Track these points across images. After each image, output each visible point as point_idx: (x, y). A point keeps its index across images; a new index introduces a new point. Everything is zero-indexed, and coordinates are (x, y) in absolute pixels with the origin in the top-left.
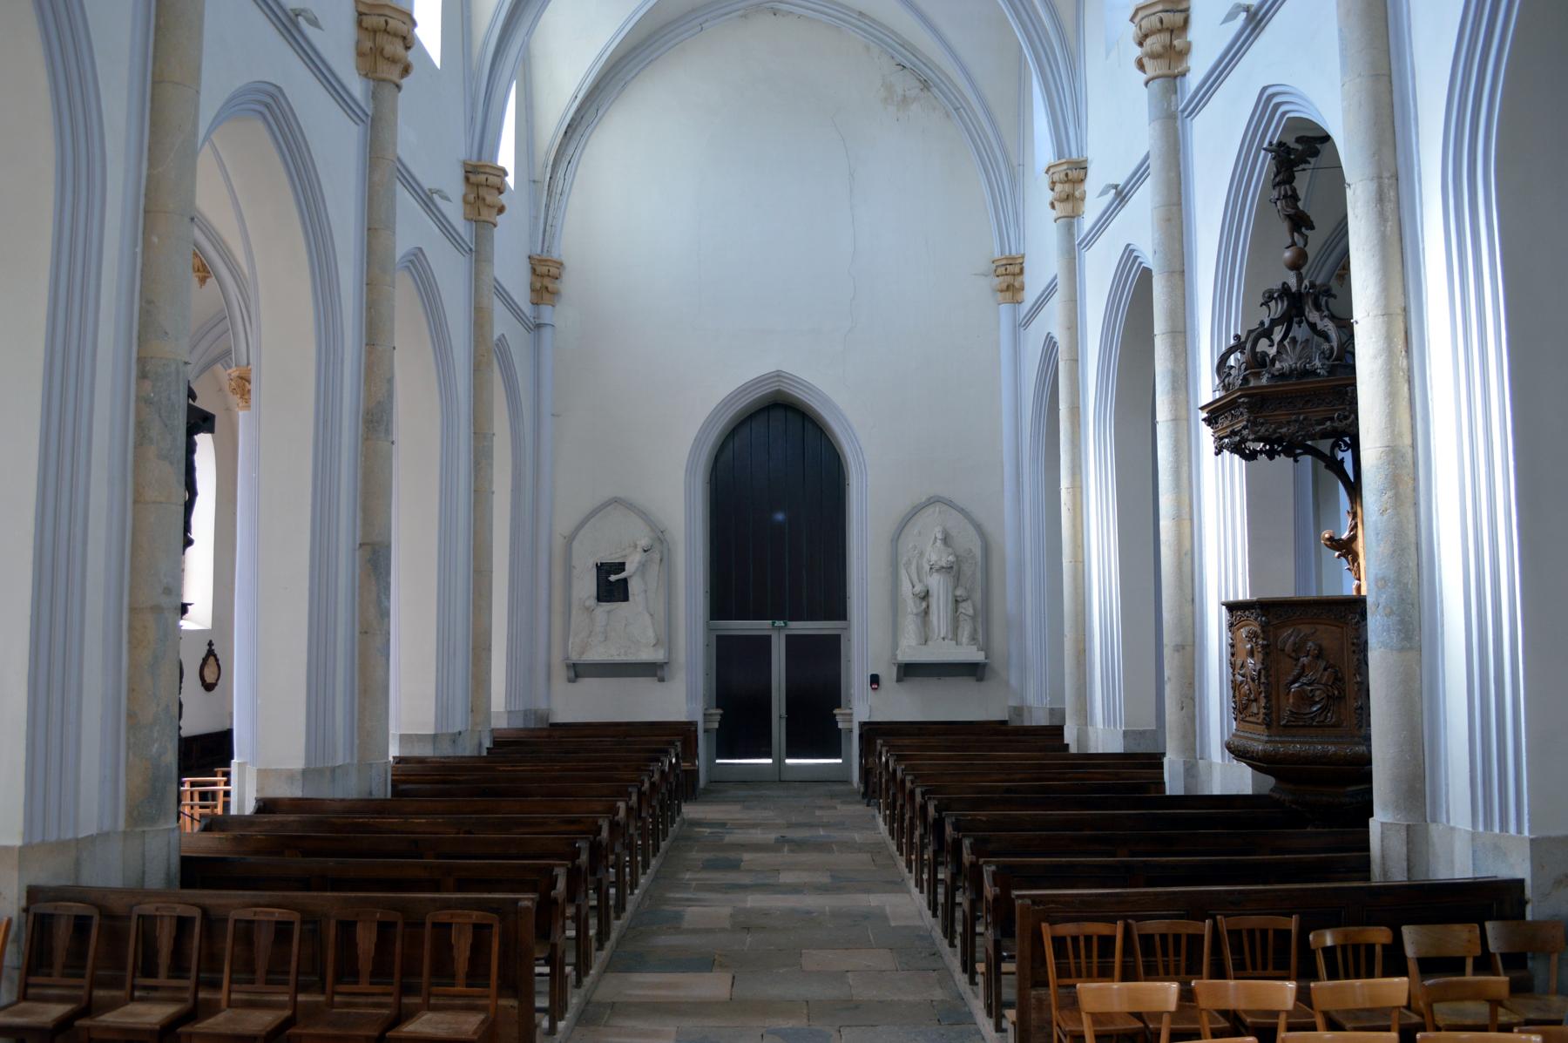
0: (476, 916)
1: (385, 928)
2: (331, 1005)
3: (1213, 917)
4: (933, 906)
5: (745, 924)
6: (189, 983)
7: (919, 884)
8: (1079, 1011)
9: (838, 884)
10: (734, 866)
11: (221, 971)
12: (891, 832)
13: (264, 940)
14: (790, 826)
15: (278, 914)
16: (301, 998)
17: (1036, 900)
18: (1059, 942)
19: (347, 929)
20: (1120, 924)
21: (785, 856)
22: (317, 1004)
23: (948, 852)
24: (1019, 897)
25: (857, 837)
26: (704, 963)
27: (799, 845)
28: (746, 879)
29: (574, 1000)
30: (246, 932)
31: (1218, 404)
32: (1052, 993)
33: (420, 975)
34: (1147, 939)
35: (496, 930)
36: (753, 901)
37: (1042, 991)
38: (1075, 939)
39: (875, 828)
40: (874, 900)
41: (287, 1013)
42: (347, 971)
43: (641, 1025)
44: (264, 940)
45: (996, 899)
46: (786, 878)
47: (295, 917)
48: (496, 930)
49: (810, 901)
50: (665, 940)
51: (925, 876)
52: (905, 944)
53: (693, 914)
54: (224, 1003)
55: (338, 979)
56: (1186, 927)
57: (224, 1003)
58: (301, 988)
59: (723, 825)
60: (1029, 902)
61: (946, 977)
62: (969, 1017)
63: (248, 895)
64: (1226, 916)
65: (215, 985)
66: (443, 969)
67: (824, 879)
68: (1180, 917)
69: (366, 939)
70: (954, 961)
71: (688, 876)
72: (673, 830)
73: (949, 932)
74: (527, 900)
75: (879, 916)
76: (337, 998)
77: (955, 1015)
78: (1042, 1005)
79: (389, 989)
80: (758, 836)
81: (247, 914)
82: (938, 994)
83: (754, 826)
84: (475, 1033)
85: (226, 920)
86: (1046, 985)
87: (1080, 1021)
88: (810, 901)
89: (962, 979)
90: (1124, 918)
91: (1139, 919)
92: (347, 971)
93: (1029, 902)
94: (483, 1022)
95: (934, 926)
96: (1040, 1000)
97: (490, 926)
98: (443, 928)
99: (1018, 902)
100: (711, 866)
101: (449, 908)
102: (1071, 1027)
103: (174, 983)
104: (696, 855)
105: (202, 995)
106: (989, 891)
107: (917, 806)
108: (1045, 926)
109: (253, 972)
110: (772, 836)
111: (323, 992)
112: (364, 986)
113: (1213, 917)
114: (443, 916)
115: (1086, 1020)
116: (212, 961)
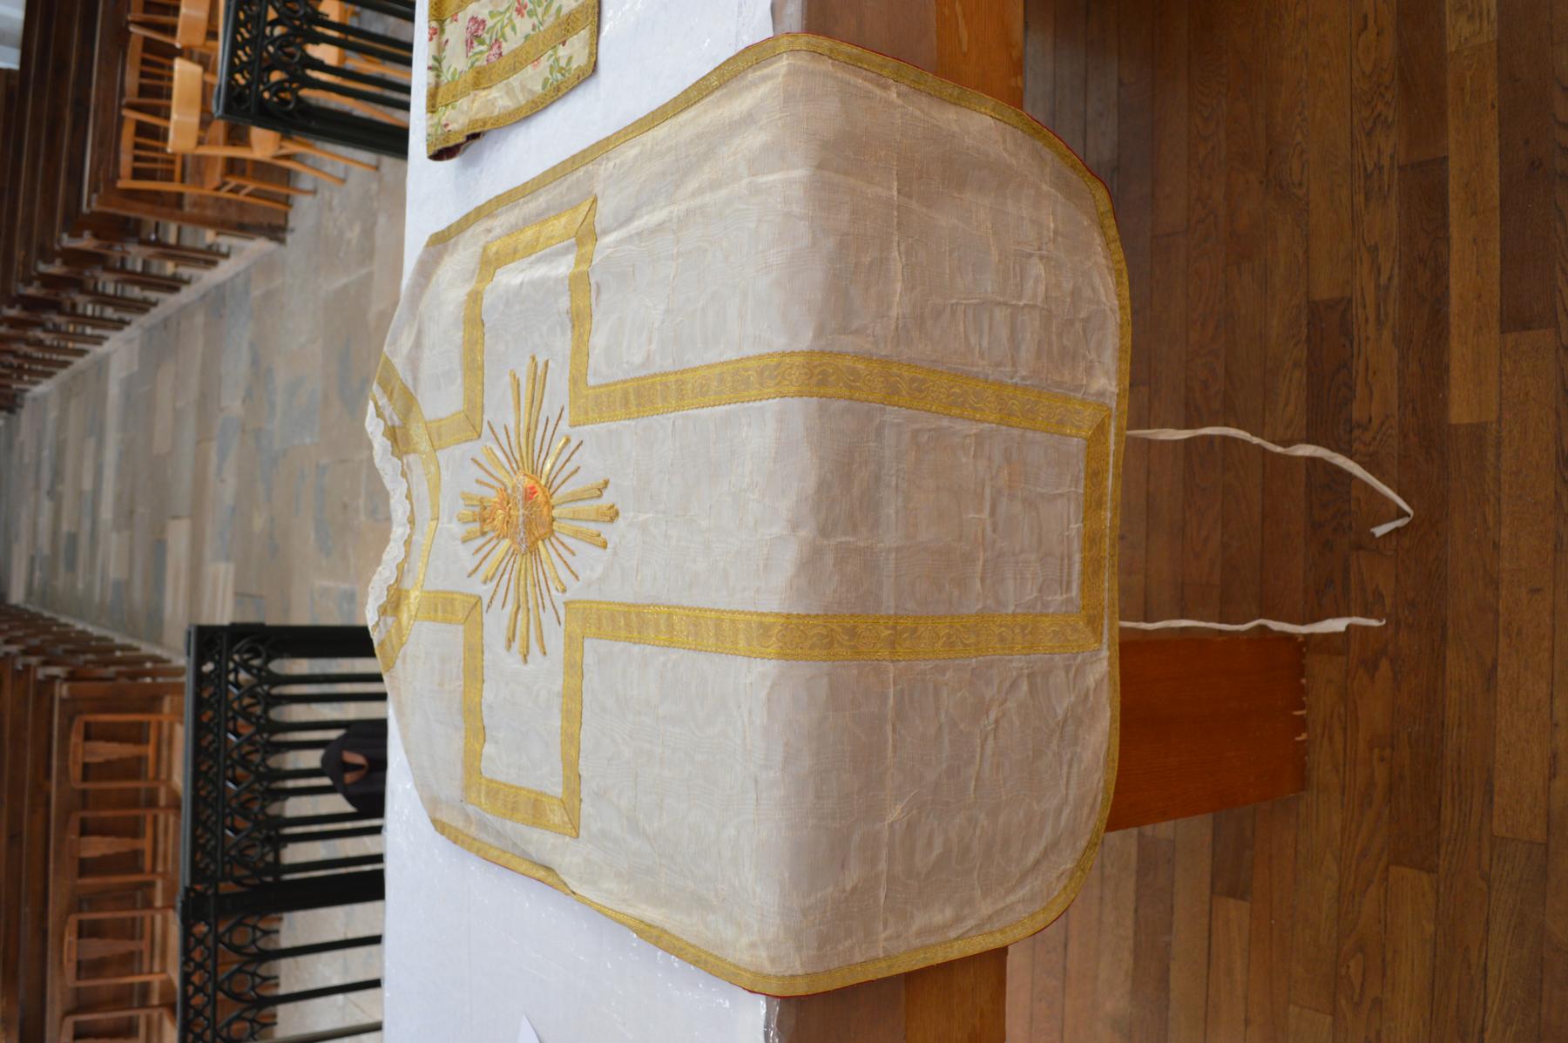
0: (76, 738)
1: (85, 831)
3: (128, 23)
4: (120, 324)
5: (126, 517)
6: (141, 1014)
7: (98, 340)
8: (199, 159)
9: (97, 430)
10: (73, 538)
11: (131, 985)
12: (49, 375)
13: (97, 948)
14: (37, 487)
15: (70, 938)
16: (159, 903)
17: (94, 189)
18: (137, 174)
19: (86, 867)
20: (127, 113)
21: (66, 489)
22: (165, 890)
23: (57, 295)
24: (89, 204)
25: (53, 415)
26: (159, 548)
27: (57, 474)
28: (87, 525)
30: (86, 968)
32: (190, 191)
33: (137, 790)
34: (143, 91)
35: (91, 718)
36: (107, 513)
37: (187, 201)
38: (137, 159)
39: (45, 396)
40: (114, 390)
42: (131, 862)
44: (97, 948)
45: (96, 236)
46: (87, 485)
47: (73, 920)
48: (91, 718)
49: (111, 456)
50: (138, 595)
51: (89, 331)
52: (157, 351)
53: (115, 571)
54: (163, 977)
55: (141, 871)
56: (135, 51)
57: (163, 977)
58: (149, 904)
59: (32, 560)
60: (94, 196)
61: (184, 309)
62: (220, 287)
63: (51, 972)
64: (129, 11)
65: (145, 989)
66: (132, 769)
67: (91, 443)
68: (125, 54)
69: (97, 847)
70: (169, 303)
71: (80, 586)
72: (32, 608)
73: (143, 307)
74: (62, 690)
75: (129, 383)
76: (160, 869)
77: (217, 301)
78: (199, 203)
79: (149, 819)
80: (45, 521)
81: (70, 969)
82: (199, 319)
83: (35, 525)
85: (78, 990)
86: (180, 196)
87: (207, 158)
88: (111, 456)
89: (186, 295)
90: (120, 107)
91: (122, 93)
92: (131, 862)
93: (94, 196)
95: (140, 322)
96: (195, 204)
97: (87, 725)
98: (88, 771)
99: (95, 207)
100: (71, 565)
101: (67, 768)
102: (215, 175)
103: (142, 1031)
104: (61, 582)
105: (155, 1000)
106: (86, 242)
107: (12, 332)
108: (121, 184)
109: (132, 954)
110: (47, 505)
111: (150, 885)
112: (145, 844)
113: (128, 23)
114: (76, 772)
115: (204, 151)
116: (122, 998)
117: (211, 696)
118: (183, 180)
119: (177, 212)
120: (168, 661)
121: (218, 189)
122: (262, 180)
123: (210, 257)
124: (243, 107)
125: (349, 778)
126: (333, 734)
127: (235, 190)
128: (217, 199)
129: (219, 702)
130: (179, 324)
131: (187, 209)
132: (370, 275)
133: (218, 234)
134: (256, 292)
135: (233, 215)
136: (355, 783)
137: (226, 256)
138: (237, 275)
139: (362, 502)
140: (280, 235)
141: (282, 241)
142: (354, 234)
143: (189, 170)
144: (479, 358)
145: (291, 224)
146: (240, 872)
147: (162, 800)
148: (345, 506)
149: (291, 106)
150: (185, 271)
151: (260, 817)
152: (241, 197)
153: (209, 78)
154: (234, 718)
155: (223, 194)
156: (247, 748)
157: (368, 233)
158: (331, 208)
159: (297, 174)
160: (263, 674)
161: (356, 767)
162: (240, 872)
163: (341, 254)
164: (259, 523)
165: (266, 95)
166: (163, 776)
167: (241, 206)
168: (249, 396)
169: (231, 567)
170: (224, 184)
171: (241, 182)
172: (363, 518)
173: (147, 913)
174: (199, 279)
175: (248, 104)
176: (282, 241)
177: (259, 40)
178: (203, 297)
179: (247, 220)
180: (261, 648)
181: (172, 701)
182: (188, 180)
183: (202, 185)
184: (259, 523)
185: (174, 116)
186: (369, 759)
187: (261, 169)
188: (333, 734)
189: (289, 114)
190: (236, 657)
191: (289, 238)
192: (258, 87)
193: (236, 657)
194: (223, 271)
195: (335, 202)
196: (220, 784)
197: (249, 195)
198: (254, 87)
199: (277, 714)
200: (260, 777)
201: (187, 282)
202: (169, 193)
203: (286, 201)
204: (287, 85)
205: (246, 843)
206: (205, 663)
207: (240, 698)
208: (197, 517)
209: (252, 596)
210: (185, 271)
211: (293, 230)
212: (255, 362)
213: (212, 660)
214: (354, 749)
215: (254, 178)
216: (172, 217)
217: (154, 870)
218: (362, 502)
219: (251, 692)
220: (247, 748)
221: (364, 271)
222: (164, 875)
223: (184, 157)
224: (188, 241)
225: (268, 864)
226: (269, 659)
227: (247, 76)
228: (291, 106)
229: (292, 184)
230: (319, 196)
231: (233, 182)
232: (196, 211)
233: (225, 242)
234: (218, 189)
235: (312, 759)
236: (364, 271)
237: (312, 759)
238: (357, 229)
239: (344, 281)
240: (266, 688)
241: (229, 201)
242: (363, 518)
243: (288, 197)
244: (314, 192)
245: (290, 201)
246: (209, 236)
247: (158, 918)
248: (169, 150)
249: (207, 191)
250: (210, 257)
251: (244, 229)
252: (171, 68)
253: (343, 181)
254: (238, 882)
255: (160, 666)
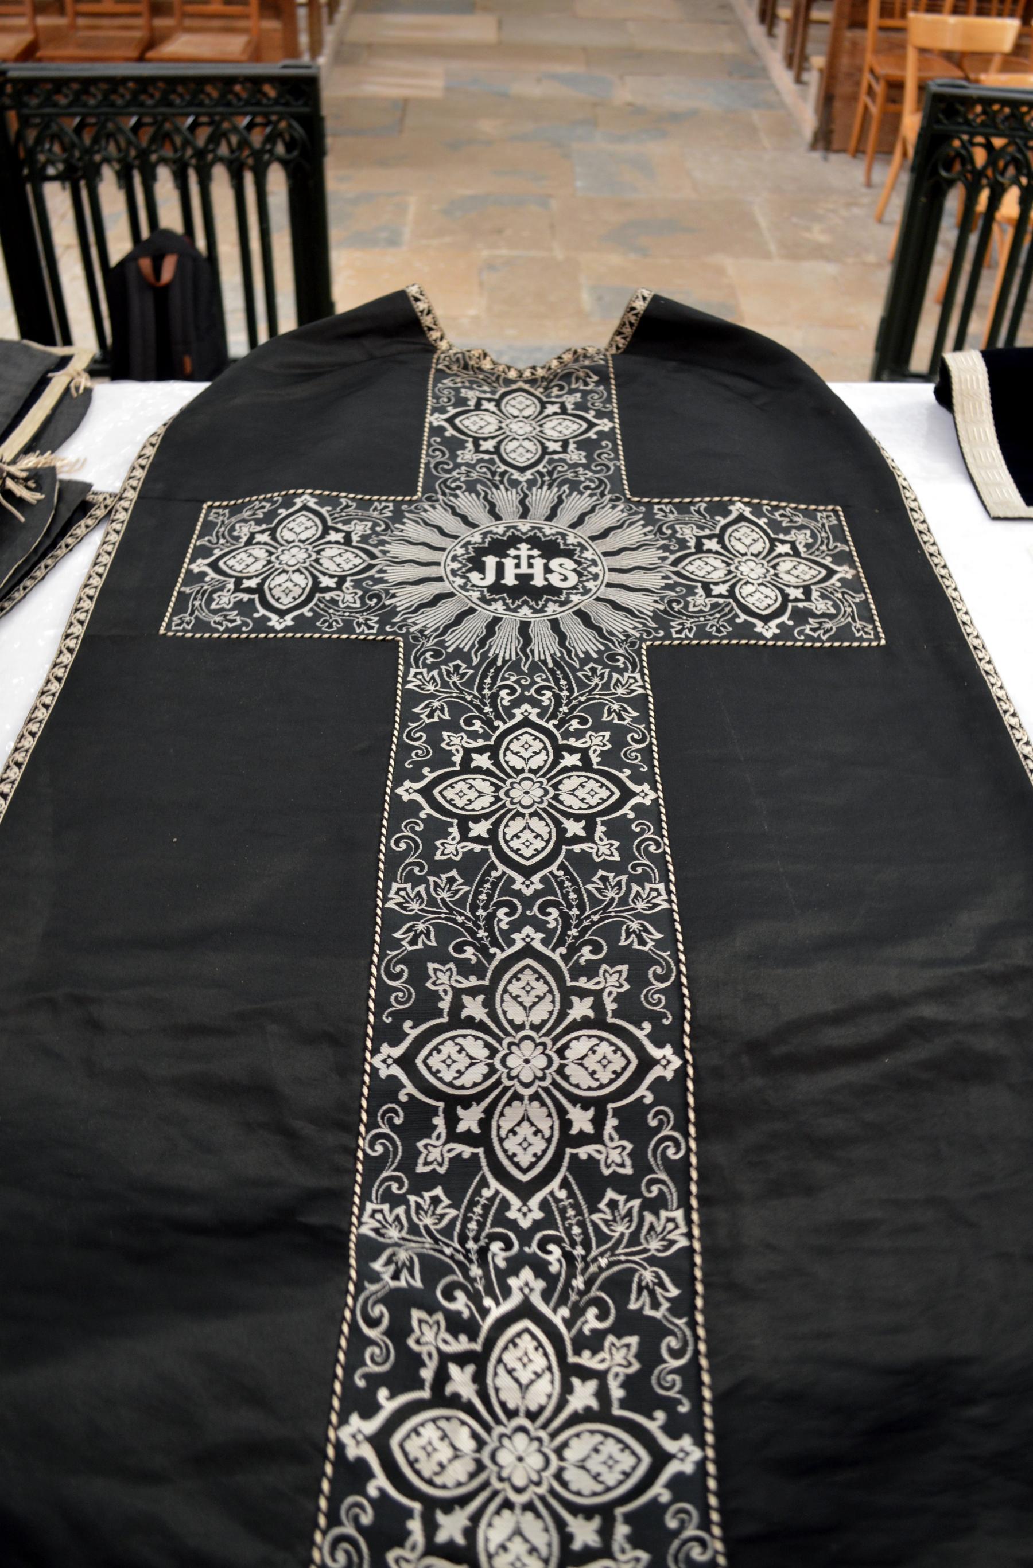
2: (73, 27)
8: (902, 46)
16: (42, 21)
22: (57, 28)
29: (329, 36)
31: (43, 263)
32: (869, 36)
41: (28, 37)
43: (404, 65)
61: (739, 28)
62: (763, 72)
76: (81, 21)
78: (856, 48)
82: (729, 48)
84: (243, 52)
87: (902, 59)
89: (756, 30)
94: (248, 43)
96: (854, 44)
102: (886, 69)
111: (61, 11)
115: (912, 56)
117: (237, 95)
118: (882, 29)
119: (845, 23)
120: (331, 20)
121: (872, 71)
122: (882, 123)
123: (796, 61)
124: (941, 116)
125: (145, 264)
126: (201, 243)
127: (870, 91)
128: (860, 70)
129: (229, 104)
130: (725, 23)
131: (849, 34)
132: (767, 256)
133: (821, 71)
134: (756, 116)
135: (843, 89)
136: (139, 271)
137: (798, 80)
138: (778, 93)
139: (504, 252)
140: (821, 144)
141: (813, 146)
142: (818, 235)
143: (893, 35)
144: (923, 199)
145: (834, 157)
146: (31, 135)
147: (160, 22)
148: (500, 231)
149: (944, 174)
150: (781, 30)
151: (97, 158)
152: (864, 98)
153: (997, 61)
154: (211, 123)
155: (867, 78)
156: (178, 140)
157: (818, 252)
158: (849, 205)
159: (888, 162)
160: (266, 157)
161: (157, 270)
162: (31, 135)
163: (794, 220)
164: (487, 126)
165: (957, 143)
166: (188, 22)
167: (854, 98)
168: (635, 110)
169: (437, 94)
170: (877, 78)
171: (880, 98)
172: (485, 253)
173: (27, 8)
174: (773, 47)
175: (945, 122)
176: (813, 146)
177: (1022, 134)
178: (754, 52)
179: (838, 105)
180: (295, 153)
181: (275, 30)
182: (882, 35)
183: (877, 52)
184: (487, 126)
185: (953, 20)
186: (168, 286)
187: (892, 122)
188: (201, 243)
189: (935, 172)
190: (283, 125)
191: (817, 155)
192: (964, 132)
193: (283, 125)
194: (782, 77)
195: (856, 211)
196: (132, 109)
197: (866, 108)
198: (965, 128)
199: (220, 176)
200: (143, 154)
201: (770, 34)
202: (866, 12)
203: (858, 151)
204: (969, 167)
205: (67, 140)
206: (274, 87)
207: (235, 129)
208: (501, 50)
209: (402, 120)
210: (781, 30)
211: (825, 159)
212: (675, 117)
213: (280, 95)
214: (180, 267)
215: (884, 113)
216: (839, 15)
217: (78, 14)
218: (504, 252)
219: (244, 143)
220: (178, 140)
221: (773, 247)
222: (73, 27)
223: (902, 30)
224: (814, 31)
225: (44, 168)
226: (285, 163)
227: (979, 120)
228: (944, 174)
229: (880, 156)
230: (864, 190)
231: (879, 89)
232: (847, 45)
233: (813, 78)
234: (872, 71)
235: (171, 218)
236: (773, 247)
237: (171, 218)
238: (823, 238)
239: (763, 222)
240: (250, 161)
241: (858, 84)
242: (485, 253)
243: (864, 152)
244: (869, 184)
245: (860, 155)
246: (818, 61)
247: (22, 22)
248: (911, 15)
249: (869, 59)
250: (796, 61)
251: (827, 100)
252: (1012, 15)
253: (880, 220)
254: (20, 136)
255: (325, 12)
